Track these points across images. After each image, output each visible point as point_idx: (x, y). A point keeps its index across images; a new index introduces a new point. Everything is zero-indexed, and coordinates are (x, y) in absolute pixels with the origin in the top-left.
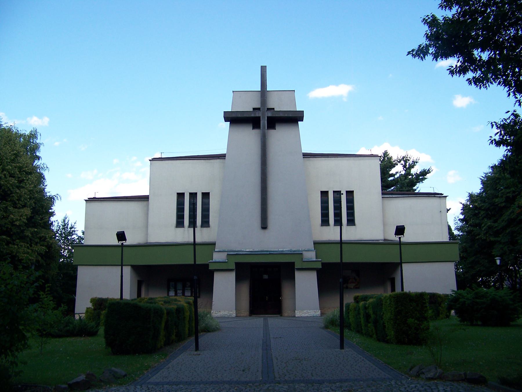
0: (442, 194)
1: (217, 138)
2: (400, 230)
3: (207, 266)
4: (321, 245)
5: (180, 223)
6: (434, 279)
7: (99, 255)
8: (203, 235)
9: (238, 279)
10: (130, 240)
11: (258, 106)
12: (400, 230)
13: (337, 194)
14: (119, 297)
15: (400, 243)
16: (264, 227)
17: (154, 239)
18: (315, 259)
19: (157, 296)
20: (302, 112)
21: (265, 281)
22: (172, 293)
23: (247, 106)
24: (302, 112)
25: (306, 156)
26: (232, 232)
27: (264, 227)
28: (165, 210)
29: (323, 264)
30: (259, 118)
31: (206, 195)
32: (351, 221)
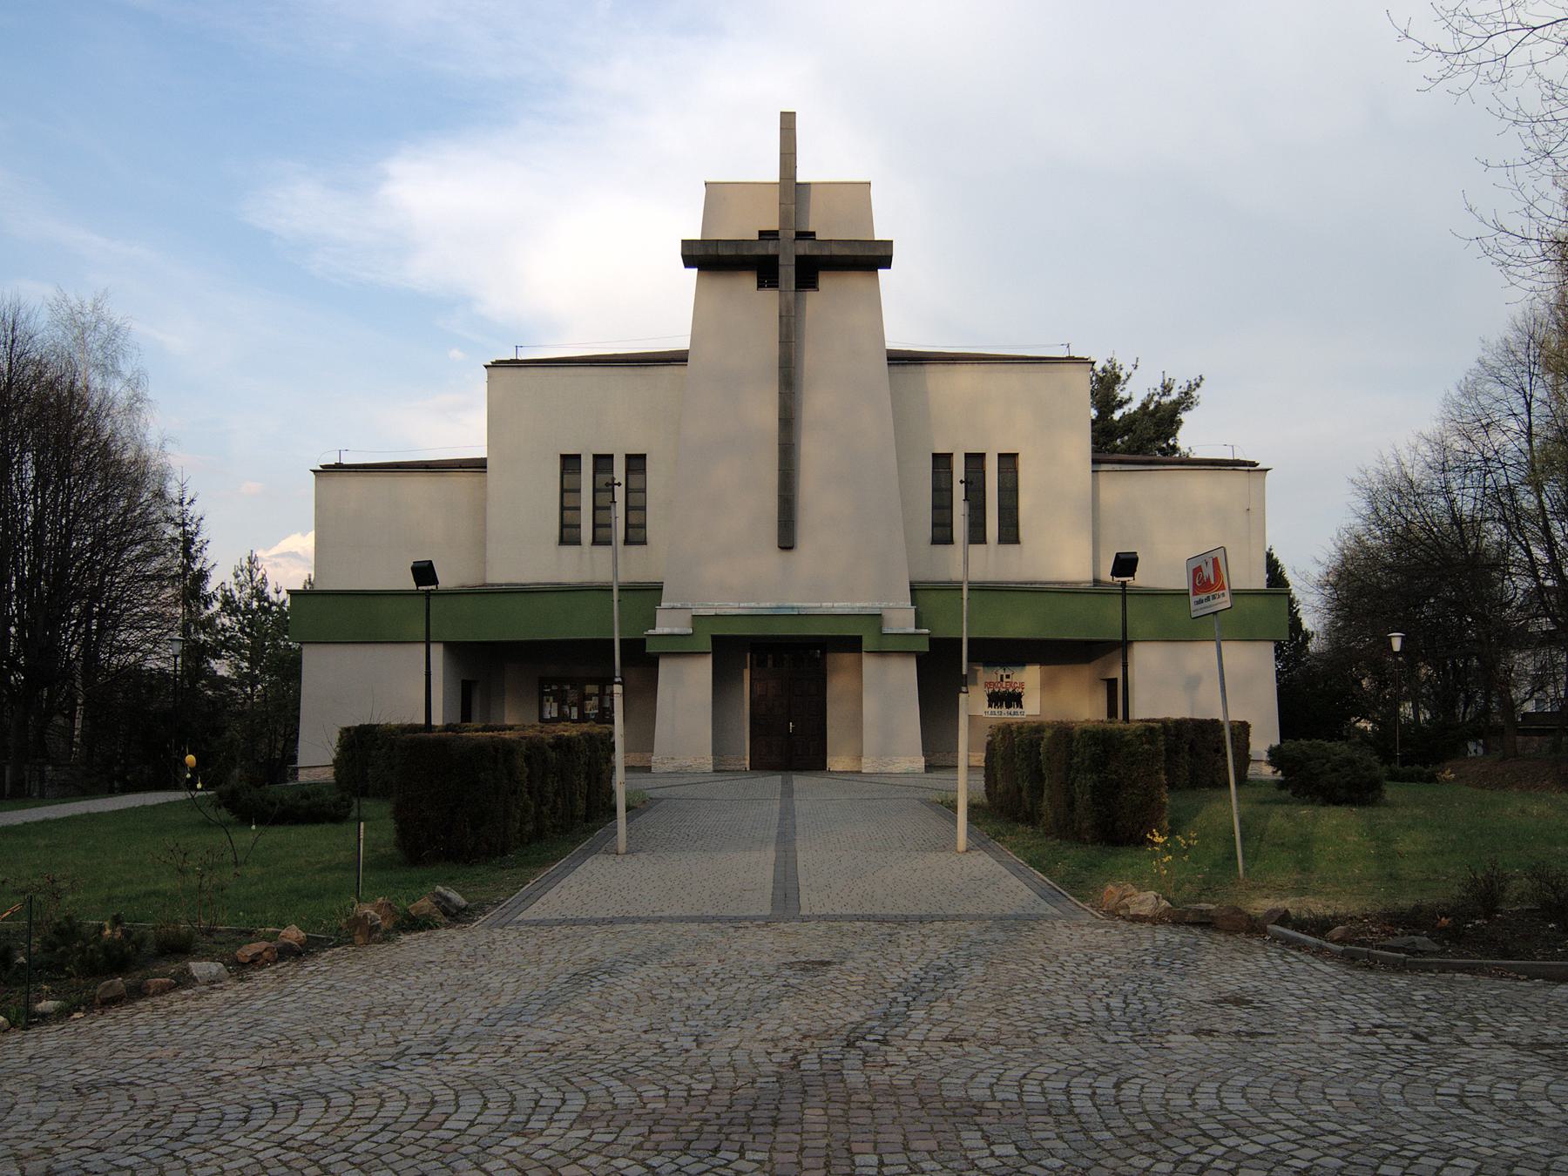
0: (1254, 464)
1: (659, 304)
2: (1125, 564)
3: (642, 642)
4: (1120, 608)
5: (568, 535)
6: (1234, 687)
7: (329, 612)
8: (634, 566)
9: (722, 680)
10: (447, 579)
11: (773, 225)
12: (1125, 564)
13: (975, 461)
14: (423, 722)
15: (1124, 591)
16: (787, 542)
17: (500, 575)
18: (912, 630)
19: (517, 718)
20: (889, 244)
21: (784, 682)
22: (551, 710)
23: (742, 227)
24: (889, 244)
25: (899, 359)
26: (713, 561)
27: (787, 542)
28: (530, 499)
29: (933, 642)
30: (775, 258)
31: (636, 462)
32: (1010, 533)
